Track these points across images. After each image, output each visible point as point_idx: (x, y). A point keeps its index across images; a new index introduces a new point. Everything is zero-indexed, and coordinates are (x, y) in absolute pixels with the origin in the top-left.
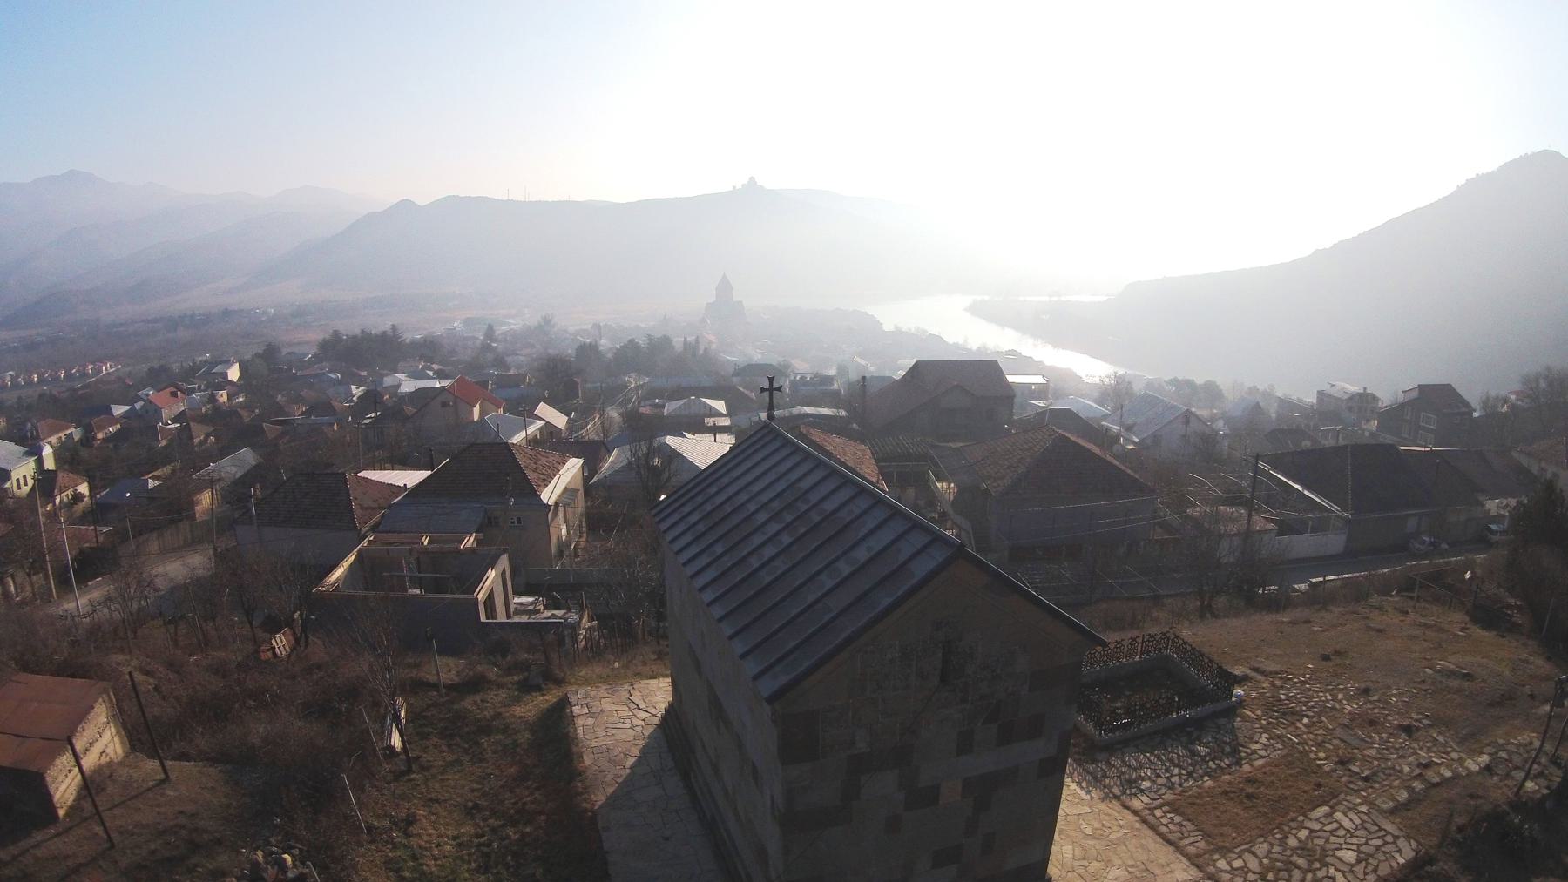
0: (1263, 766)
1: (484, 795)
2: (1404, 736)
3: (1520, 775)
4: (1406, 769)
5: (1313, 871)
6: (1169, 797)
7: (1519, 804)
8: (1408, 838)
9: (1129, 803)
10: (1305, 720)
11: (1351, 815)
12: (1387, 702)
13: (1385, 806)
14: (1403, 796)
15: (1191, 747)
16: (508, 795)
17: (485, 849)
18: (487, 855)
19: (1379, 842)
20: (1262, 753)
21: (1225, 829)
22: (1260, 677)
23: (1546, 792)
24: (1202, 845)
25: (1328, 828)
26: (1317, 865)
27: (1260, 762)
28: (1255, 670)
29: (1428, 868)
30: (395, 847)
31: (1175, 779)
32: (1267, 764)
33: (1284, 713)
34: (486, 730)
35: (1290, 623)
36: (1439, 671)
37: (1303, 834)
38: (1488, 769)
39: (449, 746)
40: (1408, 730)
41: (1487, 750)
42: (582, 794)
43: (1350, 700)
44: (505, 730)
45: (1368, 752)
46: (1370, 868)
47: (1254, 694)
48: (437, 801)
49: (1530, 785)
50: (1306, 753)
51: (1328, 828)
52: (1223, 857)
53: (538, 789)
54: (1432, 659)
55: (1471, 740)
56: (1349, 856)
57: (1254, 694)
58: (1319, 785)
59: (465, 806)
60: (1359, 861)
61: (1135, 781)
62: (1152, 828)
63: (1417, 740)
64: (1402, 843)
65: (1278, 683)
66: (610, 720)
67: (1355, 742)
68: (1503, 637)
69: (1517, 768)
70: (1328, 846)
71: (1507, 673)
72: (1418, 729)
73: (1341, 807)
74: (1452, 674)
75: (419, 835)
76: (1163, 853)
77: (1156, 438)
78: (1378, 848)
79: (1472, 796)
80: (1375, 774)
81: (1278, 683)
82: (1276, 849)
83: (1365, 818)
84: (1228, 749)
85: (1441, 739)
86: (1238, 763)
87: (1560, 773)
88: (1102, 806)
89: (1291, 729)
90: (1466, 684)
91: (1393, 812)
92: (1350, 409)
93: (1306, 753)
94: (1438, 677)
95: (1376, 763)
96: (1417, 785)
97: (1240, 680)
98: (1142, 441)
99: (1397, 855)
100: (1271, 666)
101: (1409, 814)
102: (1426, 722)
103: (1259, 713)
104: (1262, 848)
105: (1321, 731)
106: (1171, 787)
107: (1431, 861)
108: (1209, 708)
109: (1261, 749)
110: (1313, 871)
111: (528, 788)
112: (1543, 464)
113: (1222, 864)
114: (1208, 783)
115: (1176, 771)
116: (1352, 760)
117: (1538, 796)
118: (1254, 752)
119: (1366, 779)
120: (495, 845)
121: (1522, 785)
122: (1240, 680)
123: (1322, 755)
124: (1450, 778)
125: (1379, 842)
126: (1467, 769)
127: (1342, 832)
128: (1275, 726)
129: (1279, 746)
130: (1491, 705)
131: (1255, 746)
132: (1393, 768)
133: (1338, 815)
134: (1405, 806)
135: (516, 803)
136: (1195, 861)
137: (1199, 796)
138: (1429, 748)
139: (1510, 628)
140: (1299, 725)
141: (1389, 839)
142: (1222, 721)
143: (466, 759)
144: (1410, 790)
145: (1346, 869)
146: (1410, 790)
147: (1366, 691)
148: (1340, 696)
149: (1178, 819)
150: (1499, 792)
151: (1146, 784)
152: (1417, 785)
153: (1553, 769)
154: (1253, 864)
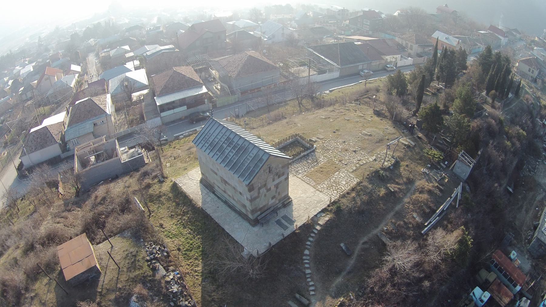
0: (323, 164)
1: (172, 212)
2: (354, 153)
3: (383, 161)
4: (355, 162)
5: (337, 186)
6: (305, 174)
7: (383, 169)
8: (356, 178)
9: (298, 176)
10: (331, 151)
11: (343, 173)
12: (349, 144)
13: (350, 171)
14: (354, 168)
15: (307, 161)
16: (178, 210)
17: (182, 223)
18: (183, 224)
19: (350, 179)
20: (322, 161)
21: (318, 179)
22: (319, 140)
23: (390, 165)
24: (314, 183)
25: (339, 177)
26: (338, 185)
27: (323, 163)
28: (318, 138)
29: (361, 184)
30: (164, 232)
31: (306, 169)
32: (324, 163)
33: (326, 150)
34: (160, 197)
35: (324, 118)
36: (363, 134)
37: (334, 179)
38: (375, 160)
39: (154, 204)
40: (355, 151)
41: (375, 155)
42: (196, 204)
43: (341, 144)
44: (164, 195)
45: (346, 158)
46: (349, 185)
47: (318, 145)
48: (162, 218)
49: (386, 163)
50: (332, 160)
51: (339, 177)
52: (319, 185)
53: (184, 206)
54: (361, 130)
55: (371, 153)
56: (344, 183)
57: (318, 145)
58: (336, 167)
59: (169, 216)
60: (346, 184)
61: (298, 171)
62: (304, 181)
63: (357, 154)
64: (355, 179)
65: (324, 142)
66: (189, 185)
67: (343, 156)
68: (382, 120)
69: (382, 159)
70: (339, 181)
71: (382, 133)
72: (357, 151)
73: (341, 172)
74: (366, 135)
75: (166, 227)
76: (308, 186)
77: (273, 36)
78: (350, 180)
79: (370, 167)
80: (348, 163)
81: (324, 142)
82: (329, 182)
83: (346, 174)
84: (315, 161)
85: (363, 153)
86: (318, 164)
87: (394, 160)
88: (293, 178)
89: (328, 154)
90: (370, 138)
91: (352, 172)
92: (339, 14)
93: (332, 160)
94: (362, 136)
95: (348, 161)
96: (358, 165)
97: (315, 142)
98: (269, 37)
99: (354, 182)
100: (321, 137)
101: (356, 172)
102: (359, 149)
103: (320, 150)
104: (326, 183)
105: (335, 154)
106: (305, 171)
107: (362, 182)
108: (309, 151)
109: (322, 160)
110: (337, 186)
111: (181, 207)
112: (407, 42)
113: (319, 187)
114: (313, 169)
115: (306, 167)
116: (343, 160)
117: (388, 166)
118: (321, 161)
119: (346, 165)
120: (183, 221)
121: (383, 163)
122: (315, 142)
123: (336, 160)
124: (365, 163)
125: (350, 179)
126: (369, 160)
127: (342, 178)
128: (324, 153)
129: (326, 159)
130: (377, 143)
131: (321, 159)
132: (352, 161)
133: (340, 174)
134: (355, 170)
135: (181, 211)
136: (314, 187)
137: (311, 173)
138: (360, 156)
139: (385, 117)
140: (330, 152)
141: (352, 178)
142: (312, 154)
143: (160, 205)
144: (356, 166)
145: (344, 185)
146: (356, 166)
147: (344, 142)
148: (338, 144)
149: (308, 178)
150: (377, 166)
151: (300, 171)
152: (358, 165)
153: (392, 159)
154: (325, 186)
